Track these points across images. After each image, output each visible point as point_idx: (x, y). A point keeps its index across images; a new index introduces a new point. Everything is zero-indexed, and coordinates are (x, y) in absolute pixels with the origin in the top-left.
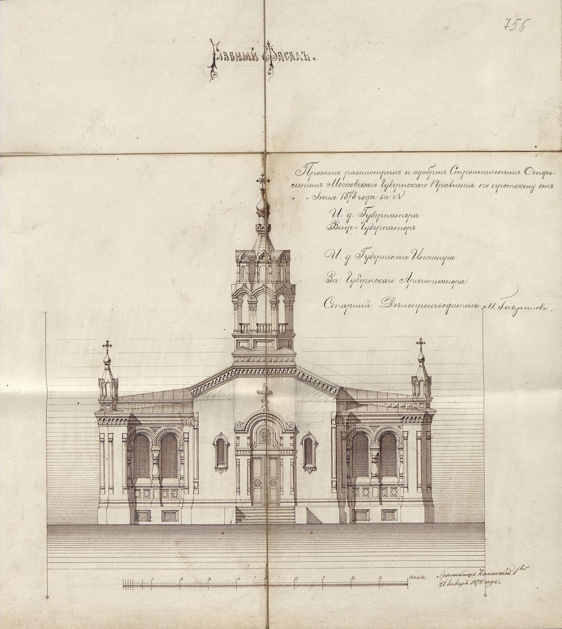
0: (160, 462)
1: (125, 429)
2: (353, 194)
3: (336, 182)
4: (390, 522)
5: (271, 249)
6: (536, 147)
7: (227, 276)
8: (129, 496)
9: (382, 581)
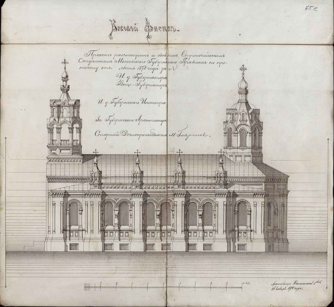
0: (202, 216)
1: (141, 200)
2: (145, 67)
3: (120, 61)
4: (109, 251)
5: (69, 99)
6: (240, 35)
7: (46, 113)
8: (143, 236)
9: (133, 286)
